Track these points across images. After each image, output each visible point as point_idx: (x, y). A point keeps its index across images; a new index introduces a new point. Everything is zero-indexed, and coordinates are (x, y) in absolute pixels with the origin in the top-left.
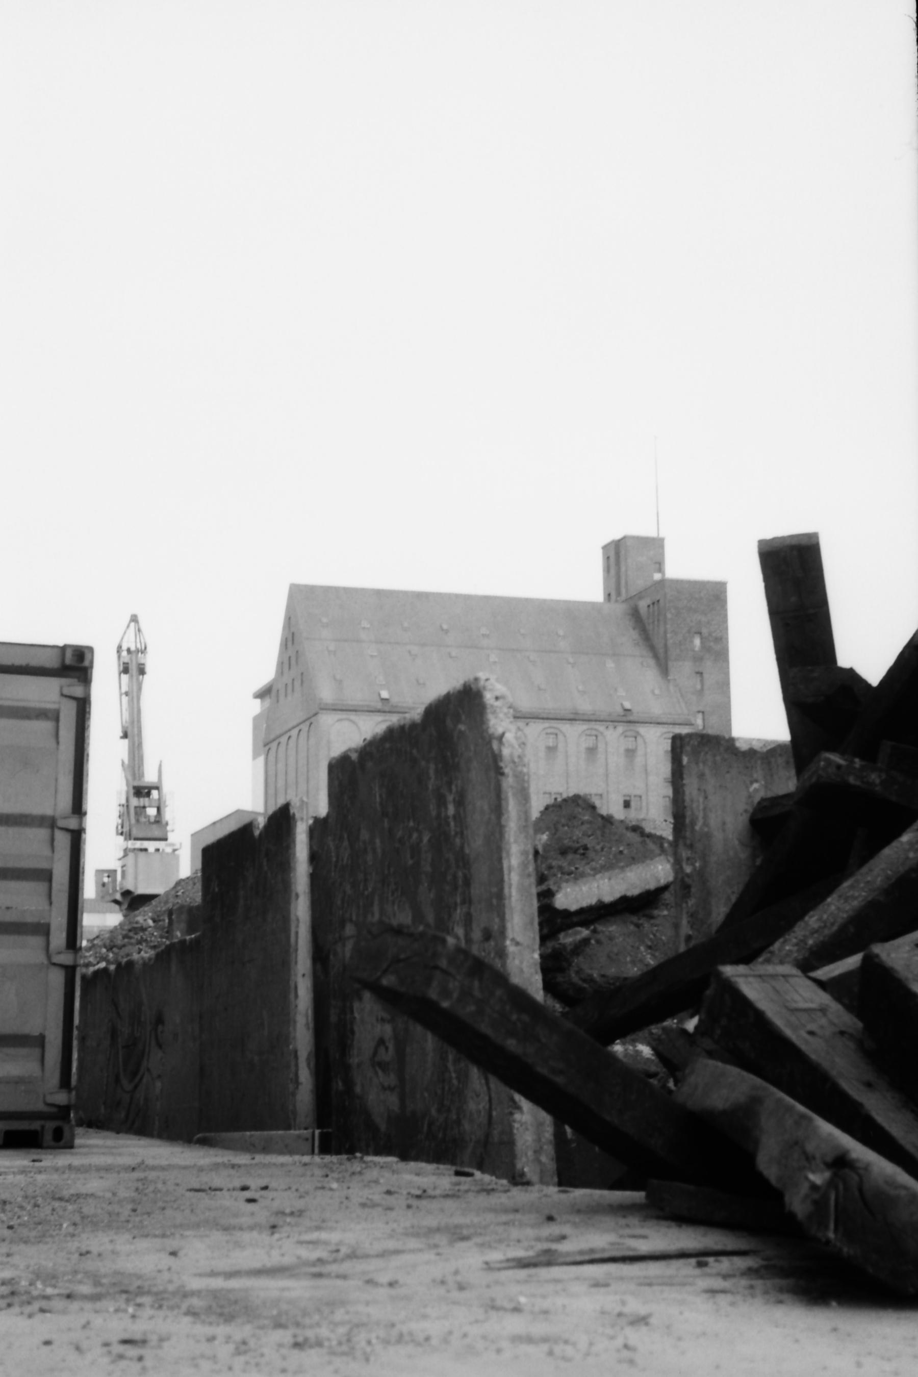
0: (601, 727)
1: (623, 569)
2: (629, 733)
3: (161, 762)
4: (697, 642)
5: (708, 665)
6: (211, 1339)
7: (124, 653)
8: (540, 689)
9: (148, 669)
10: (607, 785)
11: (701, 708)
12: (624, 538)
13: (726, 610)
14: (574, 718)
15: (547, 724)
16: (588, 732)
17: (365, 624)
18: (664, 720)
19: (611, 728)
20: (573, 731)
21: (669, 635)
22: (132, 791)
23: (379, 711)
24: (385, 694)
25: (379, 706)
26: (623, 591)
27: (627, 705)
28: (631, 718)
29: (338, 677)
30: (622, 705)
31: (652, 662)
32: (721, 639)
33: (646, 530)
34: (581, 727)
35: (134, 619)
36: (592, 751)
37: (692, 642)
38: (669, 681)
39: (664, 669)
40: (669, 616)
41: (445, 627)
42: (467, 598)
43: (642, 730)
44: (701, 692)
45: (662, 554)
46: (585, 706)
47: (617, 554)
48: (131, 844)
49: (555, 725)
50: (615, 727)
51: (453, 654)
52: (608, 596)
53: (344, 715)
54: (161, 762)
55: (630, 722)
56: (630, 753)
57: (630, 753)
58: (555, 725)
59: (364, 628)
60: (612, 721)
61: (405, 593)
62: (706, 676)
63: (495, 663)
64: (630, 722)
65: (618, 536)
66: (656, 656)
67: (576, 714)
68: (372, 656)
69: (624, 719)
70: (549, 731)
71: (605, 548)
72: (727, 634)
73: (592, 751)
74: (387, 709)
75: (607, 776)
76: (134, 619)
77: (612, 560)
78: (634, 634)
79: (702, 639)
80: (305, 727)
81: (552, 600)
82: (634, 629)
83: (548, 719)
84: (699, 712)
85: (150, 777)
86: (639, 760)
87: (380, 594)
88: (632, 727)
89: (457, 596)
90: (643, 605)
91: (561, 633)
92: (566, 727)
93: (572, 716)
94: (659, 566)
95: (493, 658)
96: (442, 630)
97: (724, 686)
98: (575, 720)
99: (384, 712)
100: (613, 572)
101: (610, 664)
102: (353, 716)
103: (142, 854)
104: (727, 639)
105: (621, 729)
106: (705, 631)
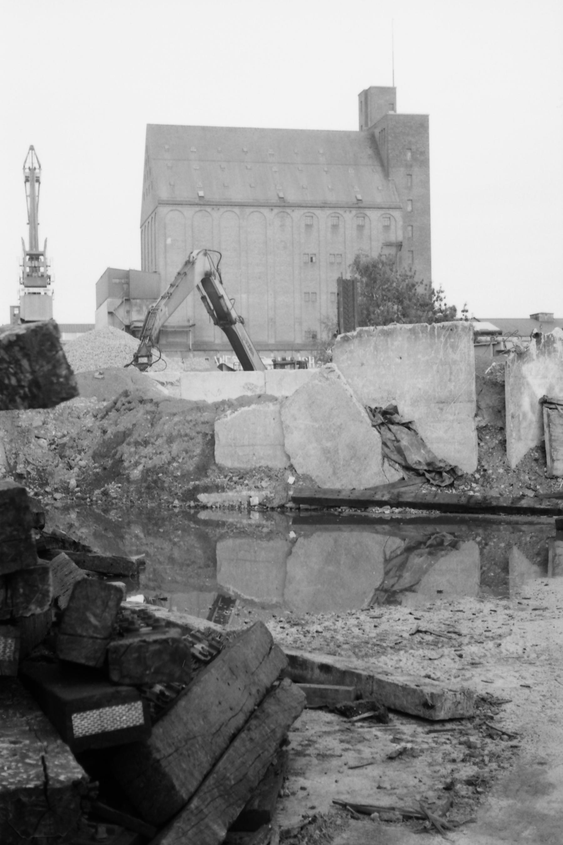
0: (340, 211)
1: (369, 109)
2: (360, 215)
3: (22, 239)
4: (409, 154)
5: (416, 170)
6: (181, 617)
7: (27, 170)
8: (303, 188)
9: (42, 180)
10: (345, 248)
11: (411, 198)
12: (370, 88)
13: (428, 134)
14: (324, 206)
15: (306, 210)
16: (333, 215)
17: (193, 149)
18: (383, 206)
19: (348, 212)
20: (374, 215)
21: (389, 151)
22: (28, 257)
23: (197, 204)
24: (201, 193)
25: (197, 201)
26: (369, 123)
27: (359, 197)
28: (360, 205)
29: (172, 183)
30: (356, 197)
31: (379, 169)
32: (424, 152)
33: (388, 84)
34: (328, 212)
35: (32, 148)
36: (335, 227)
37: (405, 155)
38: (389, 180)
39: (386, 174)
40: (390, 138)
41: (245, 150)
42: (262, 130)
43: (368, 212)
44: (410, 188)
45: (394, 98)
46: (331, 198)
47: (366, 98)
48: (27, 290)
49: (388, 212)
50: (350, 211)
51: (249, 167)
52: (361, 127)
53: (174, 207)
54: (22, 239)
55: (359, 207)
56: (360, 228)
57: (360, 228)
58: (388, 212)
59: (192, 152)
60: (349, 207)
61: (222, 129)
62: (414, 177)
63: (276, 172)
64: (359, 207)
65: (366, 88)
66: (382, 165)
67: (325, 203)
68: (196, 169)
69: (357, 206)
70: (308, 214)
71: (360, 95)
72: (428, 149)
73: (335, 227)
74: (202, 203)
75: (345, 242)
76: (32, 148)
77: (363, 103)
78: (370, 152)
79: (412, 152)
80: (153, 215)
81: (318, 131)
82: (370, 148)
83: (306, 207)
84: (409, 200)
85: (41, 249)
86: (366, 232)
87: (204, 129)
88: (362, 211)
89: (256, 129)
90: (377, 131)
91: (321, 151)
92: (318, 212)
93: (322, 205)
94: (393, 106)
95: (275, 169)
96: (243, 151)
97: (426, 183)
98: (324, 207)
99: (200, 205)
100: (364, 110)
101: (351, 171)
102: (179, 208)
103: (36, 296)
104: (428, 153)
105: (354, 212)
106: (413, 147)
